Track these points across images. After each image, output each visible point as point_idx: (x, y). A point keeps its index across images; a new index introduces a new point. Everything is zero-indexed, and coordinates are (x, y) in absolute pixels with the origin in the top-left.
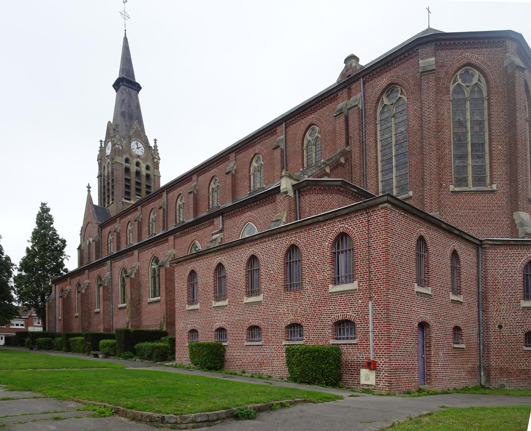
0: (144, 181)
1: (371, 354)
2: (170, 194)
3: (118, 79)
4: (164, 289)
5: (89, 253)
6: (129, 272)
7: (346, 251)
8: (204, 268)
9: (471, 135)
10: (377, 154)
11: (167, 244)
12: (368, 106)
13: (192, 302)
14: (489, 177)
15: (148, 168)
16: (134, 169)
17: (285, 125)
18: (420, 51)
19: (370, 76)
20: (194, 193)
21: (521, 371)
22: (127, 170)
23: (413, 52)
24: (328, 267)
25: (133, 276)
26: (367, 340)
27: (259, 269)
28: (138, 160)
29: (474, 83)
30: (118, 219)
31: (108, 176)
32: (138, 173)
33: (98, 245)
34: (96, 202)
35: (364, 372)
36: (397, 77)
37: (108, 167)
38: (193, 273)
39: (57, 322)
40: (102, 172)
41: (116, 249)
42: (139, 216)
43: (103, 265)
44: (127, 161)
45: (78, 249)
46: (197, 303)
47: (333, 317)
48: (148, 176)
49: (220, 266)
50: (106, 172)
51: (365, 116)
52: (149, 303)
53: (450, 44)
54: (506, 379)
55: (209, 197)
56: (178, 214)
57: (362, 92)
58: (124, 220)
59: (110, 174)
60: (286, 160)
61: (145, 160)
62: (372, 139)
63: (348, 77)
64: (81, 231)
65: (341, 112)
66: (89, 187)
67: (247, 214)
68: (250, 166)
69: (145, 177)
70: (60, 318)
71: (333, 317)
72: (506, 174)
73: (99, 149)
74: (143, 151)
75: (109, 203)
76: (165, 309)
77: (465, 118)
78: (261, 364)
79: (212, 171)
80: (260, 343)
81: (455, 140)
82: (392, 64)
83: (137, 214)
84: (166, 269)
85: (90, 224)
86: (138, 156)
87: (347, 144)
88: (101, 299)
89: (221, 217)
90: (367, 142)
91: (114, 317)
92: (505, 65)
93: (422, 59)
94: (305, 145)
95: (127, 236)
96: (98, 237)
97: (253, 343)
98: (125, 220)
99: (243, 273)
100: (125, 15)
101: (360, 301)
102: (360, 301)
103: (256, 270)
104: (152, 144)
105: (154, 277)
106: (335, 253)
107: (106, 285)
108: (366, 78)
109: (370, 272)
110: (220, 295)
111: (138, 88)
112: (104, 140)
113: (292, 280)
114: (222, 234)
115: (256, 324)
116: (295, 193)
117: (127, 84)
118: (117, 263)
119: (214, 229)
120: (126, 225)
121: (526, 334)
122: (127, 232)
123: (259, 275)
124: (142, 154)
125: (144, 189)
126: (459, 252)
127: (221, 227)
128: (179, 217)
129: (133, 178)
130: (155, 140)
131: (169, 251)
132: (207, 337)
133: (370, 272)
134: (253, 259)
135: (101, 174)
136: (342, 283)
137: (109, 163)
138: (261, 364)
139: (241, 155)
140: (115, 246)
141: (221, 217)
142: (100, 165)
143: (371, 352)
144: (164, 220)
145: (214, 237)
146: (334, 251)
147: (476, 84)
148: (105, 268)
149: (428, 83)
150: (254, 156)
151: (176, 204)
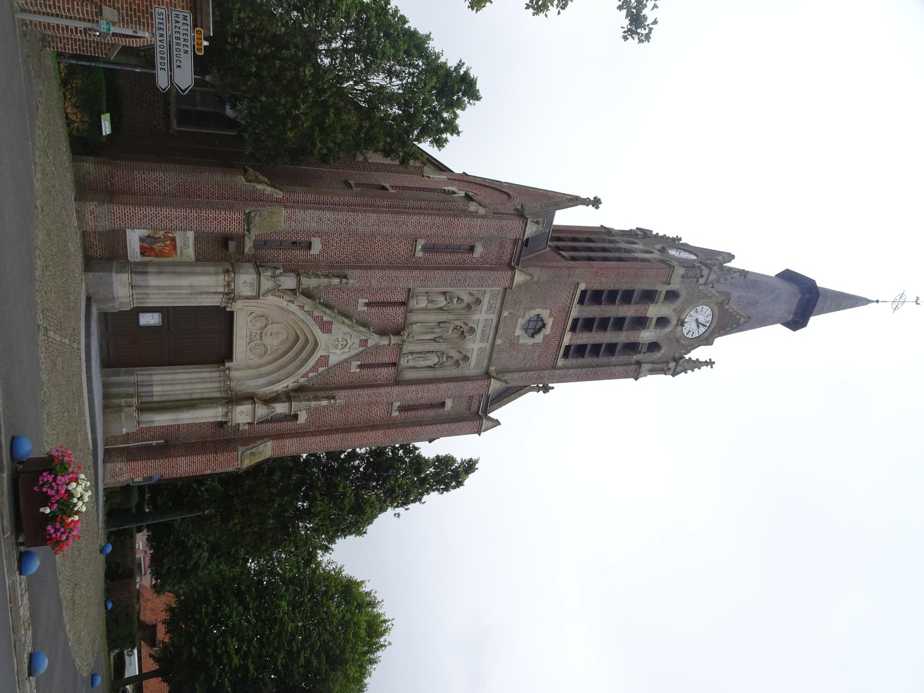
0: (622, 337)
16: (654, 311)
22: (649, 296)
28: (674, 322)
32: (641, 322)
34: (564, 218)
44: (672, 296)
66: (596, 203)
74: (689, 336)
81: (217, 13)
86: (682, 323)
100: (898, 303)
104: (698, 353)
111: (797, 322)
117: (802, 301)
124: (685, 332)
129: (629, 311)
130: (710, 363)
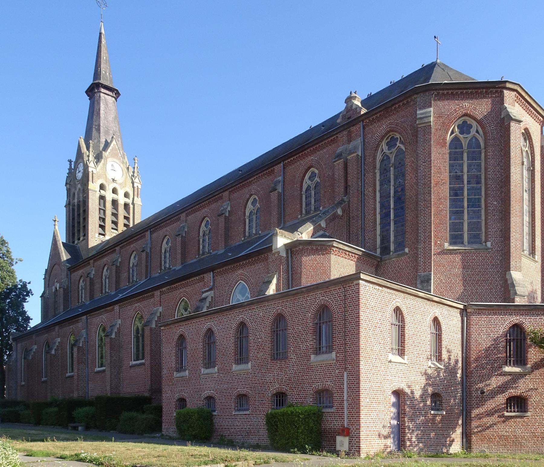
1: (345, 422)
2: (155, 235)
3: (92, 84)
4: (149, 352)
5: (55, 302)
6: (108, 329)
7: (326, 322)
8: (194, 332)
9: (468, 190)
10: (375, 205)
11: (152, 300)
12: (368, 152)
13: (180, 368)
14: (484, 234)
15: (126, 195)
16: (109, 196)
17: (284, 165)
18: (418, 99)
19: (370, 120)
20: (182, 236)
21: (500, 437)
23: (411, 100)
24: (310, 337)
25: (113, 336)
26: (343, 408)
27: (248, 337)
29: (472, 134)
30: (92, 261)
31: (79, 206)
32: (115, 203)
33: (67, 292)
35: (339, 439)
36: (396, 125)
37: (78, 194)
38: (182, 337)
39: (19, 388)
40: (71, 200)
41: (88, 298)
42: (117, 260)
43: (77, 322)
45: (41, 297)
46: (185, 370)
47: (314, 386)
48: (126, 206)
49: (210, 332)
50: (76, 200)
51: (364, 164)
52: (131, 367)
53: (447, 93)
54: (487, 445)
55: (199, 241)
56: (163, 259)
57: (362, 138)
58: (98, 263)
59: (81, 204)
60: (284, 204)
61: (123, 185)
62: (370, 189)
63: (348, 118)
64: (45, 275)
65: (339, 156)
67: (240, 271)
68: (245, 207)
69: (123, 207)
70: (23, 383)
71: (314, 386)
72: (501, 231)
73: (68, 171)
75: (79, 239)
76: (149, 375)
77: (462, 172)
78: (248, 433)
79: (203, 210)
80: (248, 412)
82: (391, 110)
83: (114, 256)
84: (151, 329)
85: (56, 266)
87: (346, 192)
88: (75, 362)
89: (212, 273)
90: (366, 192)
91: (90, 382)
92: (502, 116)
93: (420, 109)
94: (304, 190)
95: (102, 283)
96: (67, 282)
97: (241, 413)
98: (100, 263)
99: (232, 340)
101: (337, 372)
102: (337, 372)
103: (245, 337)
105: (137, 337)
106: (317, 324)
107: (81, 345)
108: (366, 122)
109: (346, 344)
110: (209, 363)
112: (74, 160)
113: (279, 352)
114: (213, 292)
115: (244, 393)
116: (287, 253)
118: (94, 320)
119: (204, 286)
120: (101, 270)
121: (507, 399)
122: (102, 278)
123: (247, 342)
125: (121, 221)
126: (440, 319)
127: (212, 284)
128: (165, 262)
131: (155, 309)
132: (194, 404)
133: (346, 344)
134: (242, 325)
135: (69, 202)
136: (323, 353)
137: (80, 189)
138: (248, 433)
139: (236, 195)
140: (88, 295)
141: (212, 273)
142: (68, 191)
143: (345, 420)
144: (147, 266)
145: (204, 295)
146: (315, 322)
147: (474, 136)
148: (80, 325)
149: (424, 136)
150: (250, 197)
151: (161, 247)
